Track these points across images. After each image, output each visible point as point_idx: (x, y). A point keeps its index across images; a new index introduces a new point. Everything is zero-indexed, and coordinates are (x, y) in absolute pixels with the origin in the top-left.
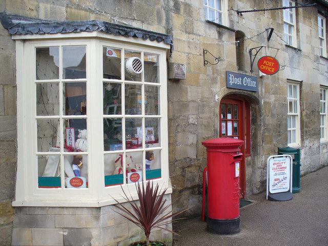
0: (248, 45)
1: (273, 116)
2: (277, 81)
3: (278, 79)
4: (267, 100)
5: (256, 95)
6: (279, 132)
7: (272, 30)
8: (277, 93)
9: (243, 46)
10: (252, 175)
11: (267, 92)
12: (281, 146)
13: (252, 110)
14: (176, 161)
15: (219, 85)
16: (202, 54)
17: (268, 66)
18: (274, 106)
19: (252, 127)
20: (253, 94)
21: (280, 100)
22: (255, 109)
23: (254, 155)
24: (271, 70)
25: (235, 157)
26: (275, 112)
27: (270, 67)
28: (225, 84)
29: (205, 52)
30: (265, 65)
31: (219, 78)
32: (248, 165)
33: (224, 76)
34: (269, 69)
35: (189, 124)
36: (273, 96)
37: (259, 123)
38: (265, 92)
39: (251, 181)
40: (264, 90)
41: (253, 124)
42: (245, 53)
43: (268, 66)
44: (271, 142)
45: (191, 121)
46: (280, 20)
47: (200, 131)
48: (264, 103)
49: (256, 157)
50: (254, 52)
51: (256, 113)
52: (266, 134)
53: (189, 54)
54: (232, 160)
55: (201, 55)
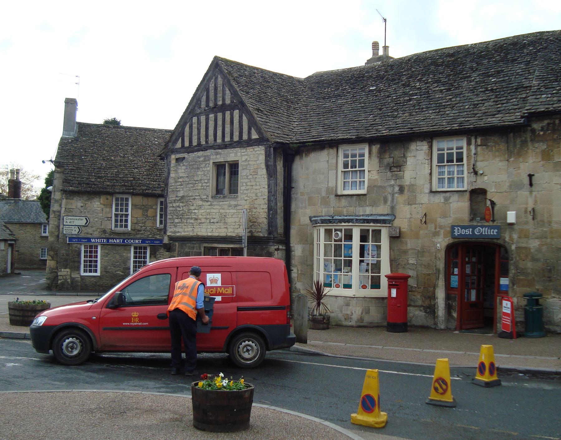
1: (534, 260)
45: (411, 262)
47: (420, 269)
48: (517, 248)
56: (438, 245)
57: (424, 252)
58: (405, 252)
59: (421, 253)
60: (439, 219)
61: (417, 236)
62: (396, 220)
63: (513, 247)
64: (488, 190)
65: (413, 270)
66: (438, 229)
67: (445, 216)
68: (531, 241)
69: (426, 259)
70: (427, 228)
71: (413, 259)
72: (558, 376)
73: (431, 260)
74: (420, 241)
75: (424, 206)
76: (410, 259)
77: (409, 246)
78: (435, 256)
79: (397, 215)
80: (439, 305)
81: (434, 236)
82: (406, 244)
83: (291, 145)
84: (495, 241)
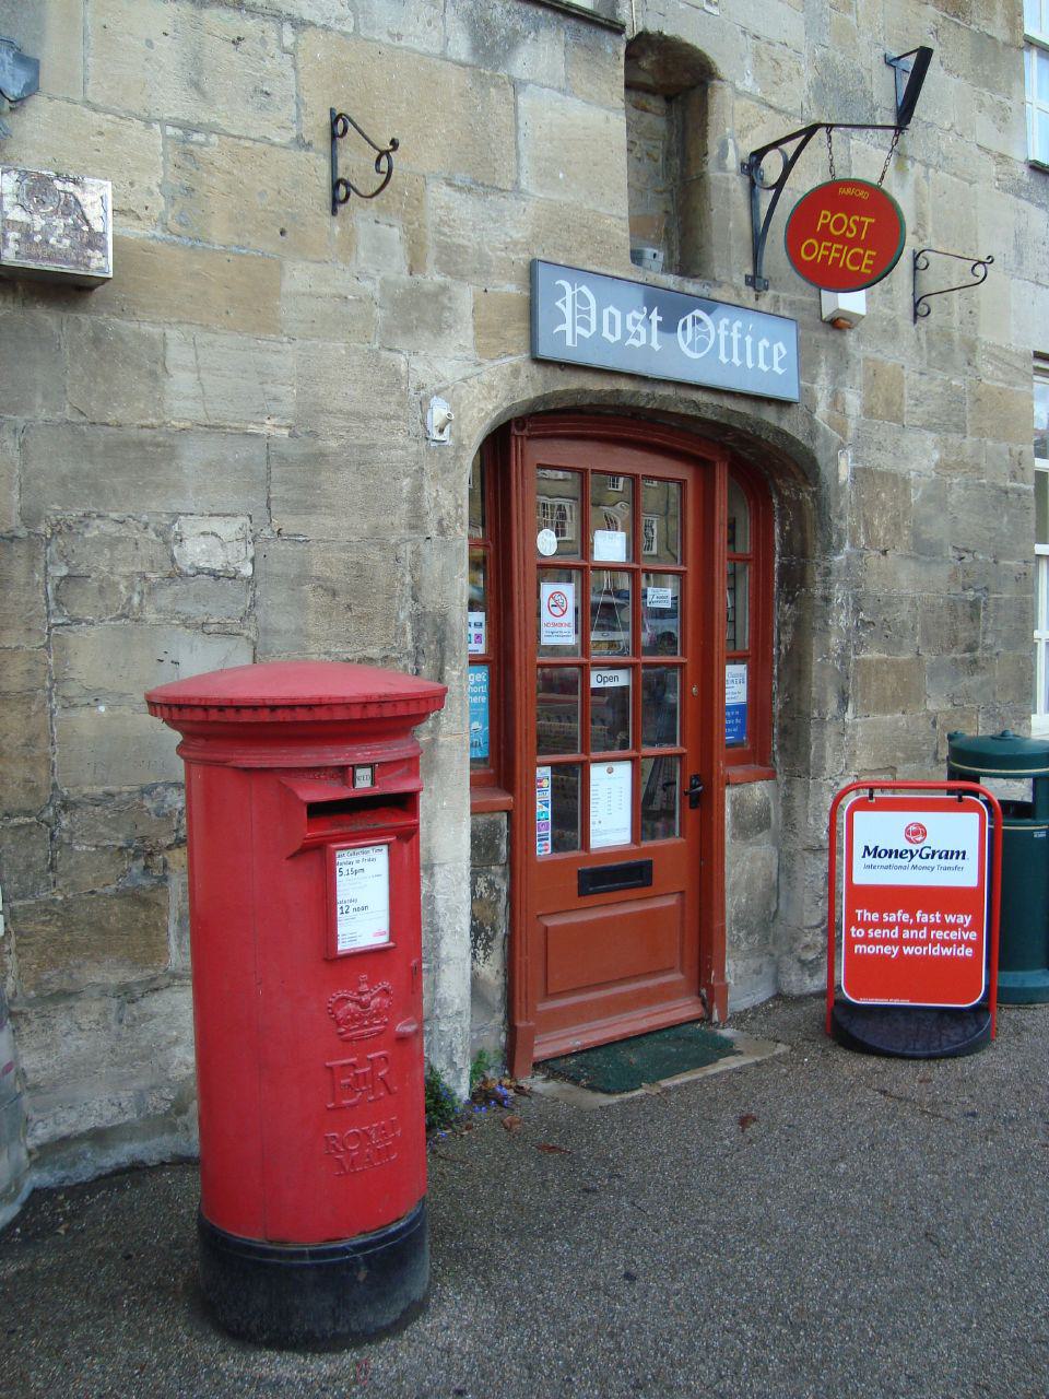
0: (740, 122)
1: (924, 550)
2: (960, 357)
3: (971, 347)
4: (883, 461)
5: (790, 424)
6: (971, 648)
7: (924, 55)
8: (960, 428)
9: (704, 136)
10: (777, 889)
11: (885, 408)
12: (978, 728)
13: (783, 518)
14: (67, 806)
15: (464, 335)
16: (323, 144)
17: (842, 239)
18: (937, 496)
19: (783, 611)
20: (769, 415)
21: (977, 468)
22: (798, 506)
23: (792, 776)
24: (857, 260)
25: (317, 810)
26: (938, 530)
27: (852, 243)
28: (527, 347)
29: (338, 126)
30: (824, 235)
31: (465, 297)
32: (744, 831)
33: (512, 289)
34: (846, 260)
35: (176, 575)
36: (930, 438)
37: (818, 592)
38: (869, 412)
39: (768, 920)
40: (853, 401)
41: (791, 599)
42: (713, 173)
43: (842, 239)
44: (905, 696)
45: (196, 551)
46: (999, 20)
47: (282, 622)
48: (862, 474)
49: (798, 783)
50: (772, 166)
51: (803, 530)
52: (872, 655)
53: (188, 128)
54: (305, 832)
55: (302, 144)
56: (439, 411)
57: (318, 459)
58: (149, 454)
59: (291, 472)
60: (439, 194)
61: (254, 304)
62: (40, 112)
63: (845, 470)
64: (723, 67)
65: (225, 633)
66: (433, 278)
67: (482, 184)
68: (910, 441)
69: (332, 533)
70: (348, 246)
71: (228, 529)
72: (702, 978)
73: (376, 538)
74: (285, 359)
75: (315, 47)
76: (187, 526)
77: (185, 392)
78: (415, 501)
79: (51, 55)
80: (443, 923)
81: (408, 330)
82: (156, 372)
83: (842, 191)
84: (769, 415)
